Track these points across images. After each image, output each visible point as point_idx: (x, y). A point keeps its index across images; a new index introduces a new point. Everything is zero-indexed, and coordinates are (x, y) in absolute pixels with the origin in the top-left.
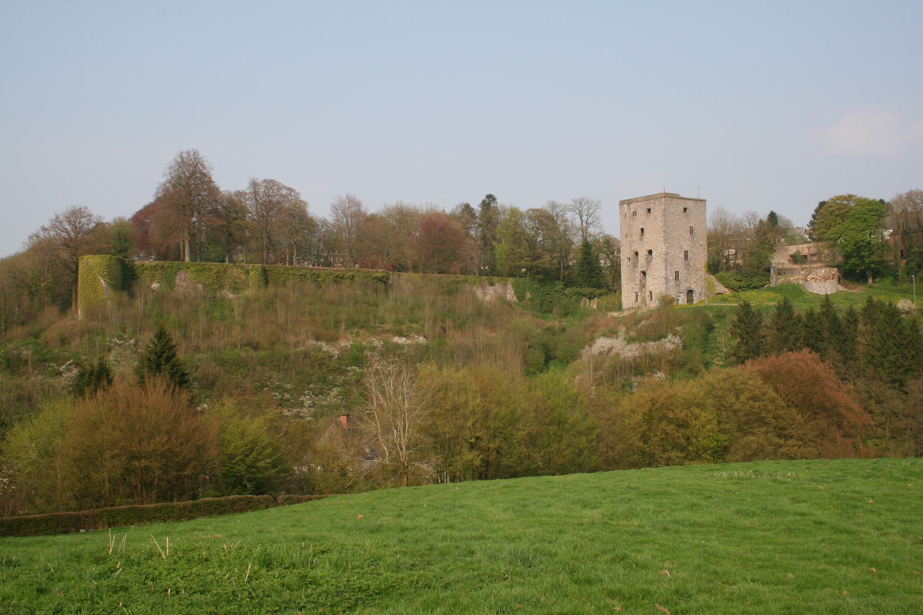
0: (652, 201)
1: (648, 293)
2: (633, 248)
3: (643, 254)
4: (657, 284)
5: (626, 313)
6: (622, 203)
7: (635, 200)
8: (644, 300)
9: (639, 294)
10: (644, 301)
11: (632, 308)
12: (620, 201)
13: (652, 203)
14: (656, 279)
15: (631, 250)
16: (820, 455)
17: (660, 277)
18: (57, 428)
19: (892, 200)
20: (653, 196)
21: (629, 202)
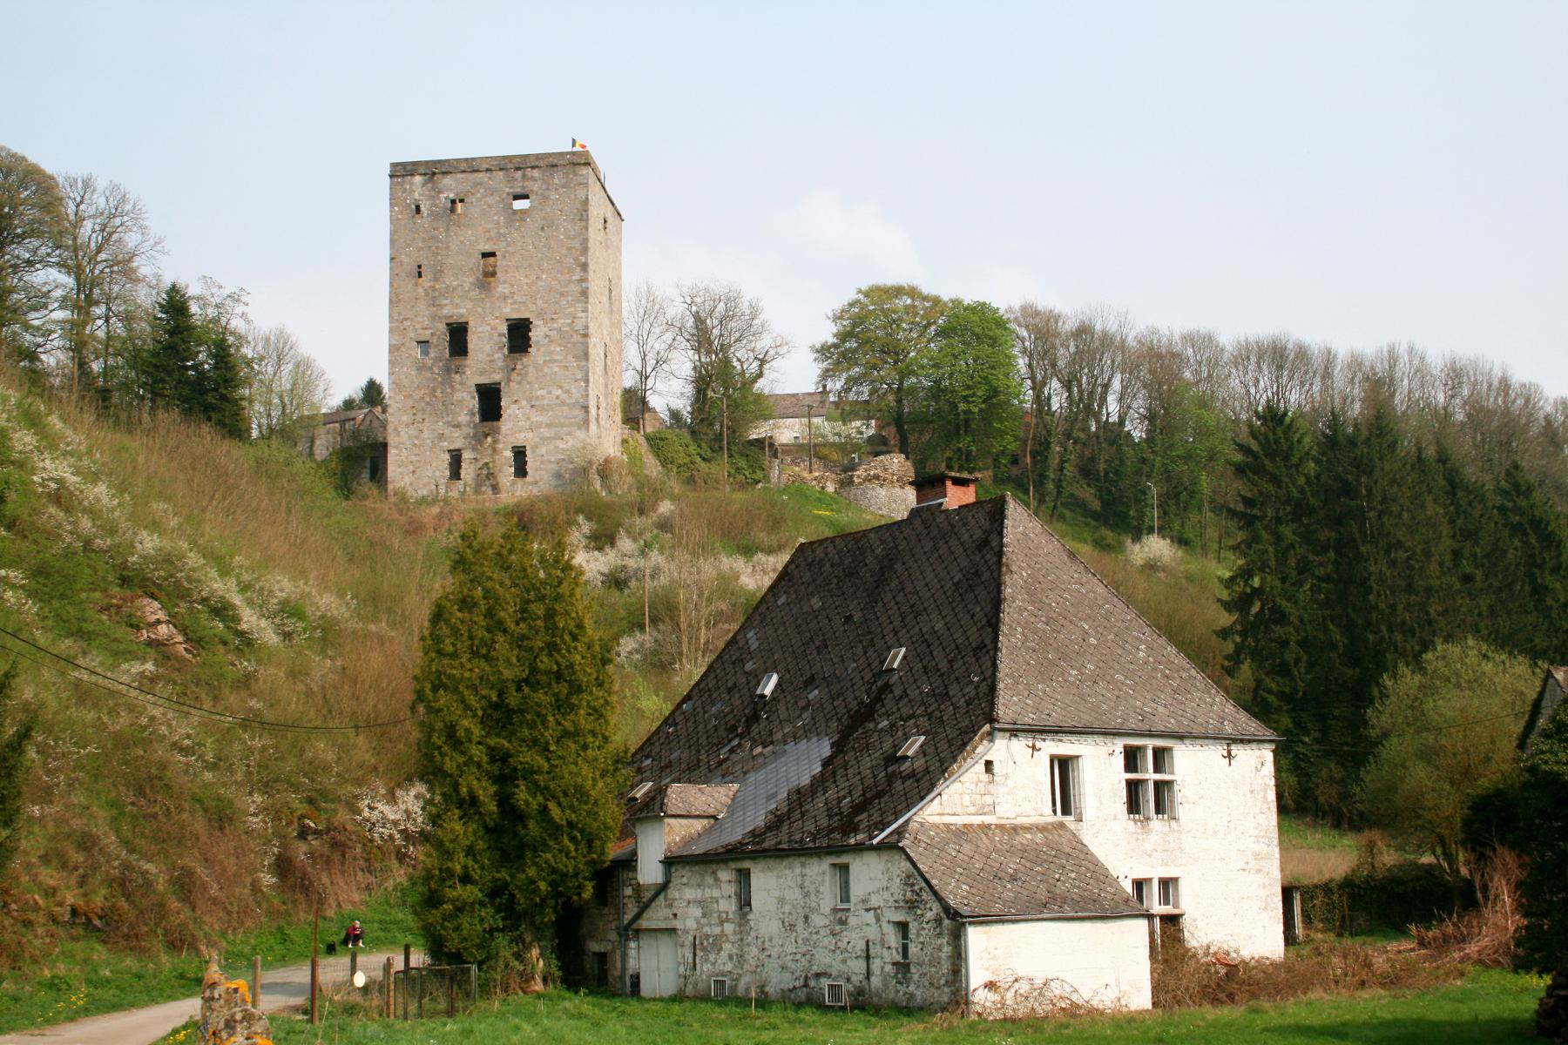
0: (536, 173)
1: (509, 454)
2: (446, 312)
3: (486, 341)
4: (549, 426)
5: (733, 865)
6: (401, 172)
7: (463, 166)
8: (490, 475)
9: (467, 455)
10: (488, 477)
11: (435, 501)
12: (394, 165)
13: (534, 179)
14: (542, 409)
15: (434, 318)
16: (1015, 829)
17: (563, 403)
18: (859, 477)
19: (1043, 328)
20: (538, 157)
21: (433, 171)
